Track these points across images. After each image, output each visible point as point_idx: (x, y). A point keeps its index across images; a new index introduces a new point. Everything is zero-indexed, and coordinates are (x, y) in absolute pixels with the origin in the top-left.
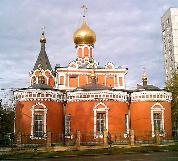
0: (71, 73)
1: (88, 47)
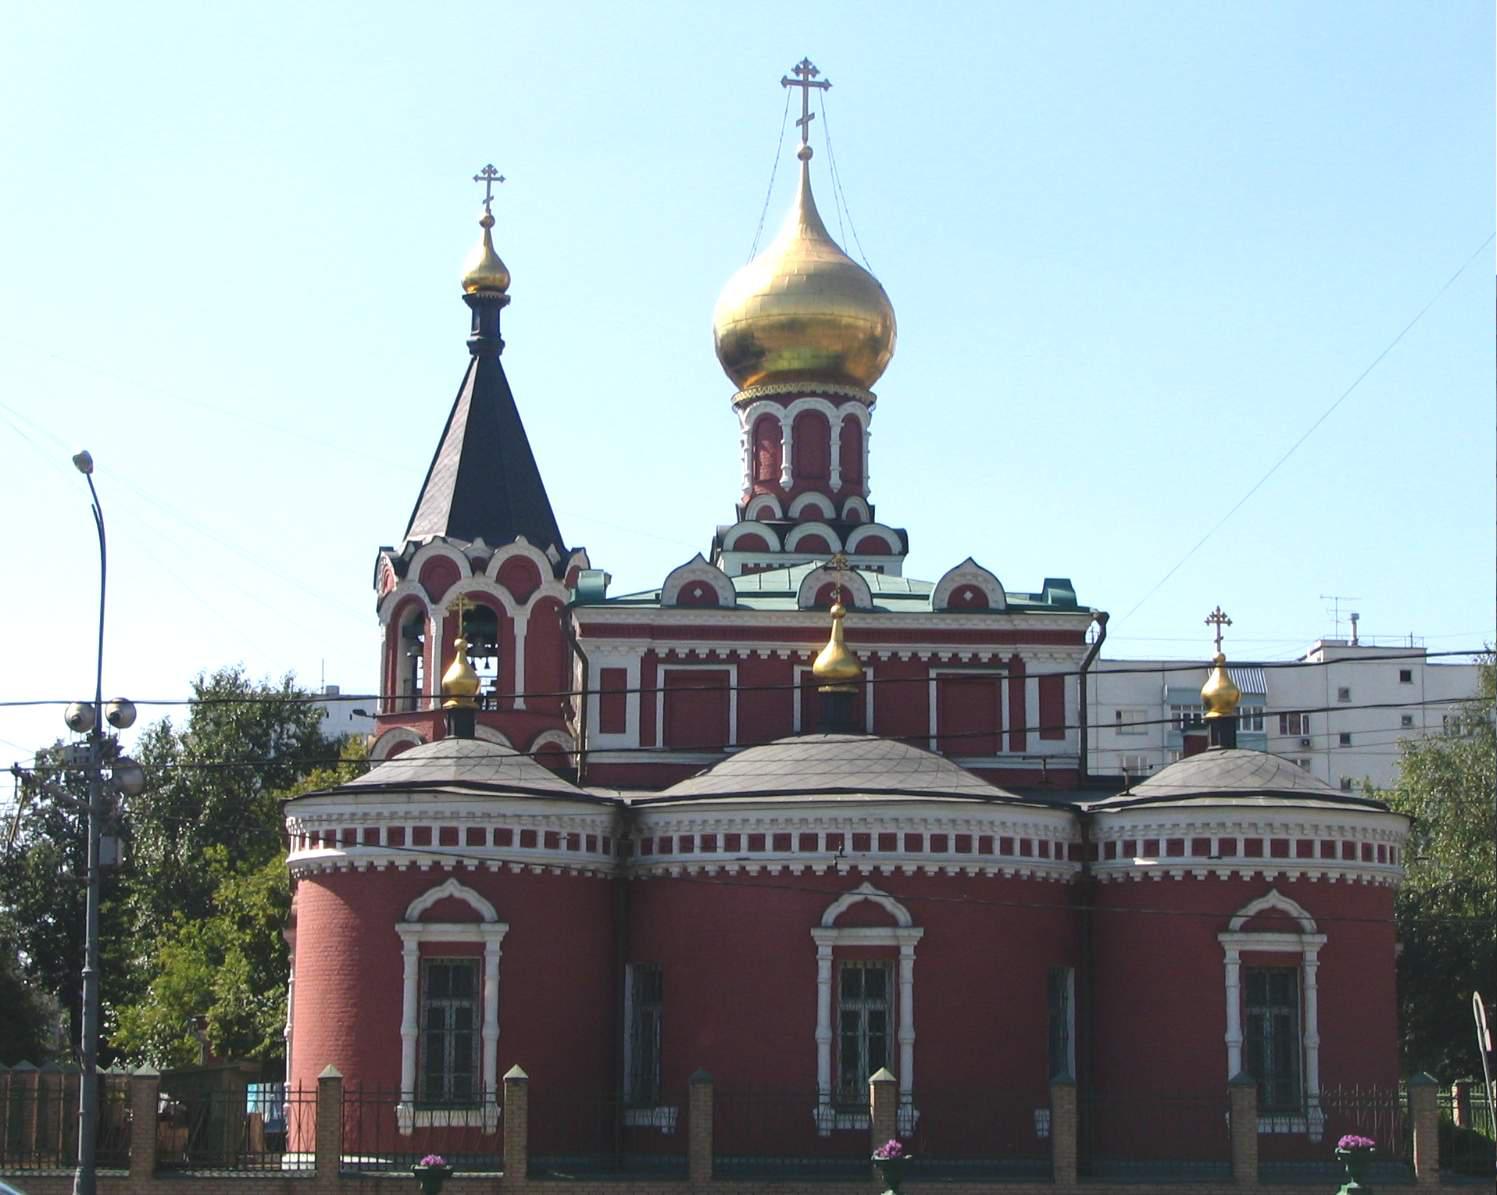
0: (682, 647)
1: (822, 405)
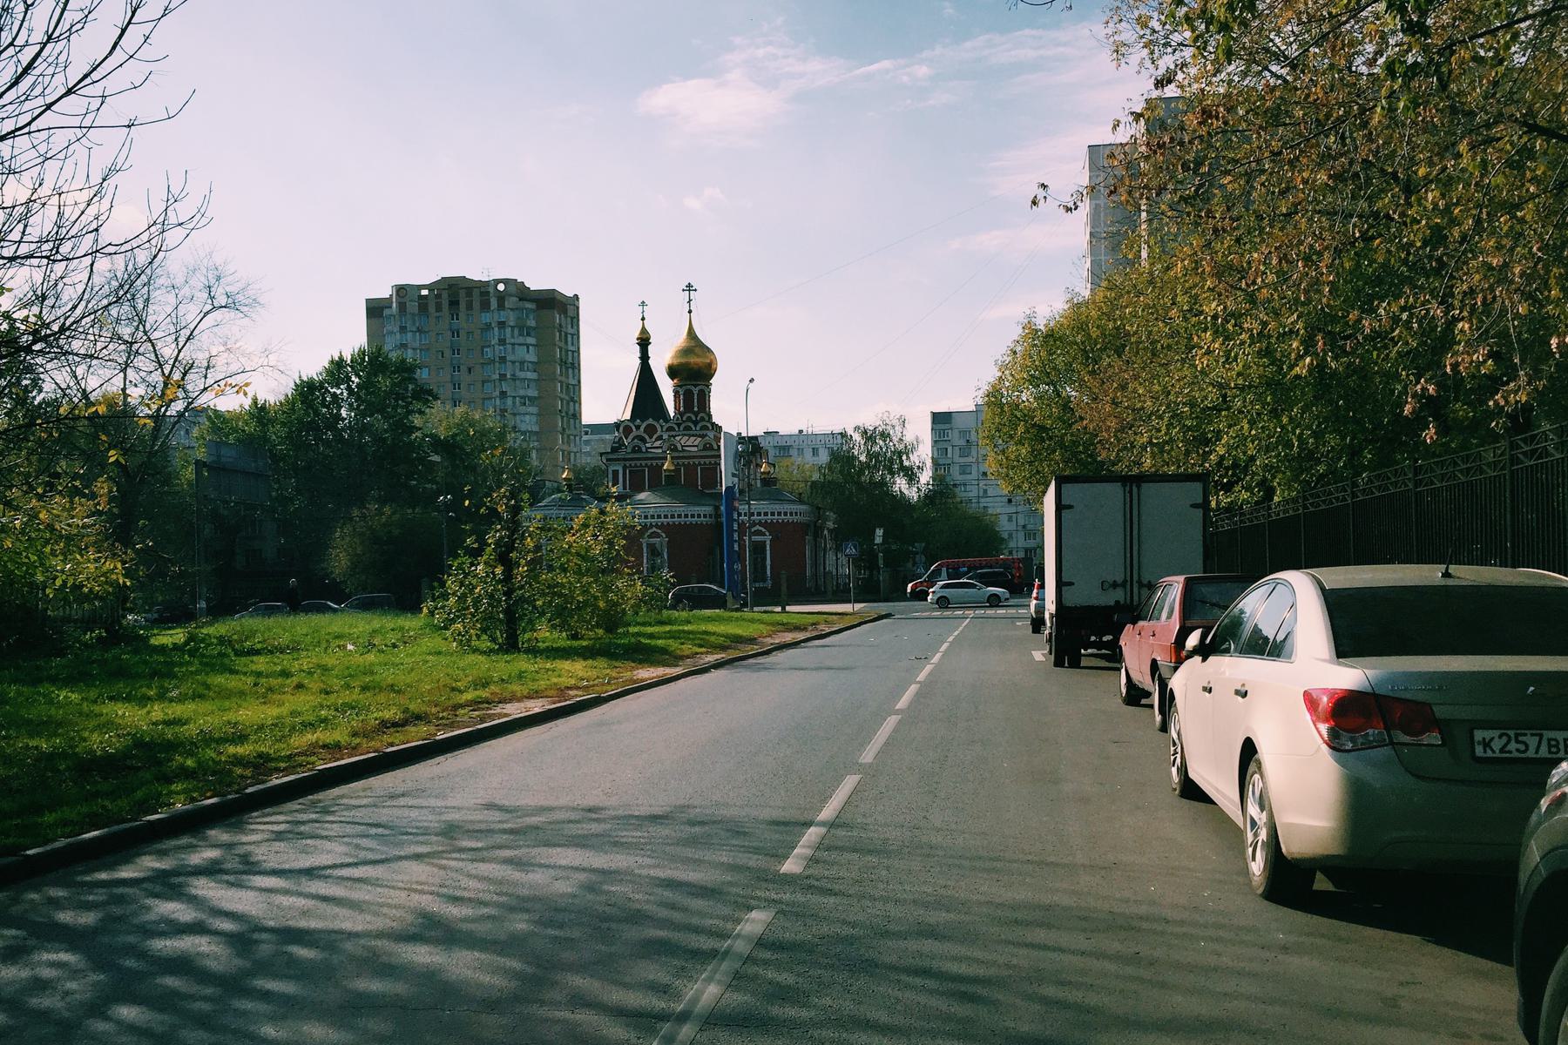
0: (633, 463)
